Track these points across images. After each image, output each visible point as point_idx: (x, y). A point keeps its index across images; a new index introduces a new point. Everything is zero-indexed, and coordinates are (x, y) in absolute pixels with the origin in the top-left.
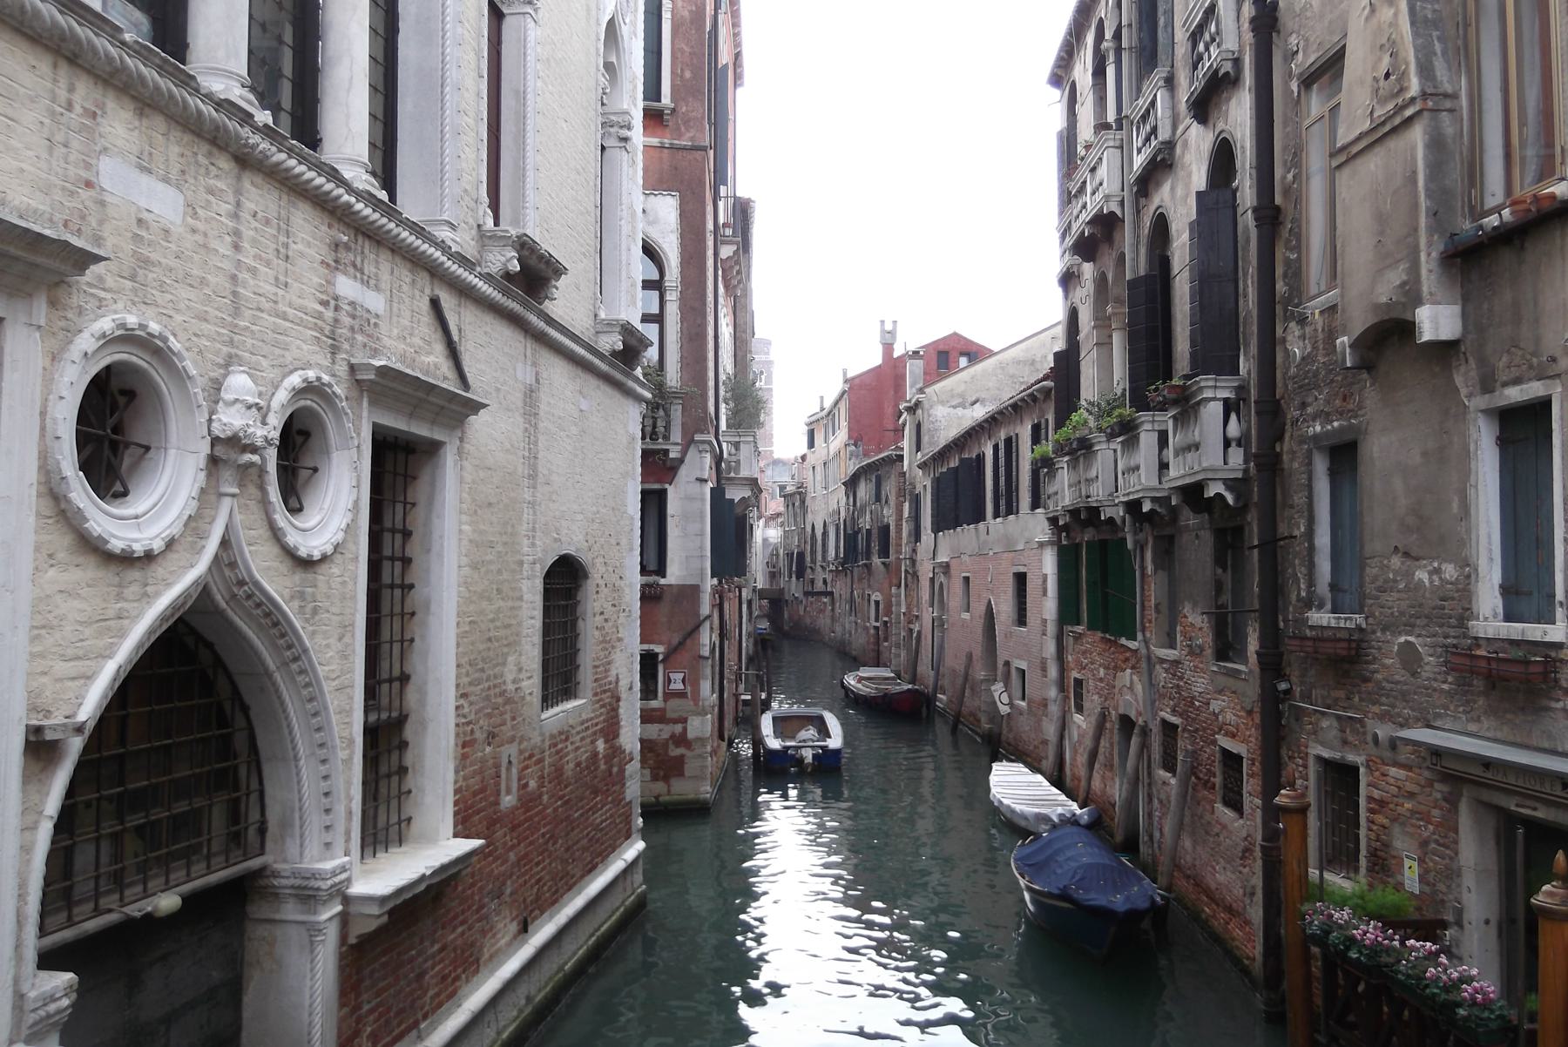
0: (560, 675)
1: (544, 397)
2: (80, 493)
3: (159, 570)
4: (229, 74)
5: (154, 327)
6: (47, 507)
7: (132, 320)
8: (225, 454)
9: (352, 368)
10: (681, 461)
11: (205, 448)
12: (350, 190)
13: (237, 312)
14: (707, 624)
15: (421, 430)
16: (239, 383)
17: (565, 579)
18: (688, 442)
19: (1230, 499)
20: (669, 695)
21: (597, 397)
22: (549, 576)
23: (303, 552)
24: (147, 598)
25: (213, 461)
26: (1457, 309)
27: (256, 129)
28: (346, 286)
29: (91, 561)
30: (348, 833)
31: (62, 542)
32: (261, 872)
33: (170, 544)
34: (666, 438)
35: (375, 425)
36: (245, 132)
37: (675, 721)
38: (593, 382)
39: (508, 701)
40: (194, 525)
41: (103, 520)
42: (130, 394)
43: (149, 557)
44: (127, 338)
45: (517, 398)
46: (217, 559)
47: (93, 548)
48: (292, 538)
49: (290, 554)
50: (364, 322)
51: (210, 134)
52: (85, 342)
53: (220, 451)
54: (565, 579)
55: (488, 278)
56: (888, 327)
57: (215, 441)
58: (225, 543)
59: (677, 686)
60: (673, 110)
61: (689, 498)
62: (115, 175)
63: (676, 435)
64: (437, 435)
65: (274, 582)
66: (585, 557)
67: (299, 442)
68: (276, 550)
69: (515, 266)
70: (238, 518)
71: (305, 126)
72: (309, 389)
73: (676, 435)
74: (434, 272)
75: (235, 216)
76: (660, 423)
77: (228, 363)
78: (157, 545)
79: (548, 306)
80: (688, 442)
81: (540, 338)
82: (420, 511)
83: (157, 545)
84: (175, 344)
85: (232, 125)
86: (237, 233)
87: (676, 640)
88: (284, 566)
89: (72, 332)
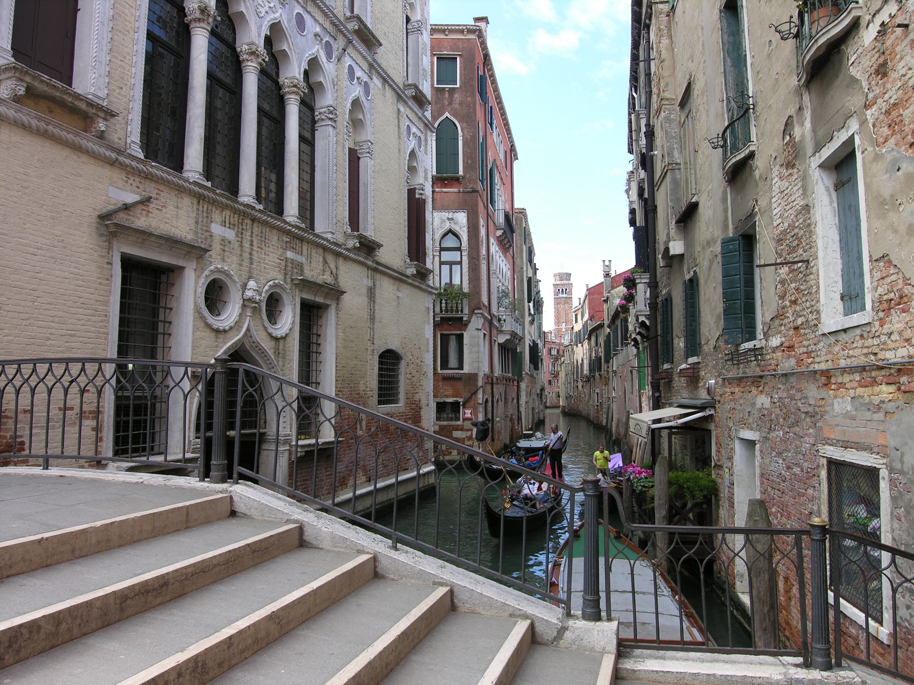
0: (387, 392)
1: (377, 292)
2: (206, 313)
3: (228, 335)
4: (250, 196)
5: (226, 268)
6: (197, 315)
7: (219, 266)
8: (247, 303)
9: (292, 280)
10: (469, 321)
11: (241, 302)
12: (290, 225)
13: (252, 264)
14: (481, 390)
15: (320, 299)
16: (252, 284)
17: (389, 360)
18: (472, 312)
19: (648, 323)
20: (465, 419)
21: (406, 293)
22: (381, 356)
23: (274, 335)
24: (225, 343)
25: (244, 306)
26: (682, 242)
27: (257, 211)
28: (290, 254)
29: (209, 330)
30: (291, 425)
31: (201, 325)
32: (265, 433)
33: (231, 328)
34: (462, 311)
35: (302, 299)
36: (253, 212)
37: (468, 430)
38: (414, 289)
39: (361, 397)
40: (238, 324)
41: (211, 319)
42: (221, 287)
43: (225, 331)
44: (218, 271)
45: (364, 291)
46: (245, 333)
47: (209, 326)
48: (271, 330)
49: (270, 335)
50: (300, 266)
51: (244, 214)
52: (207, 272)
53: (246, 303)
54: (389, 360)
55: (347, 249)
56: (607, 263)
57: (244, 300)
58: (248, 330)
59: (468, 415)
60: (463, 177)
61: (473, 337)
62: (217, 229)
63: (466, 311)
64: (180, 263)
65: (267, 345)
66: (400, 351)
67: (273, 304)
68: (265, 333)
69: (358, 245)
70: (252, 323)
71: (279, 208)
72: (276, 286)
73: (466, 311)
74: (325, 249)
75: (251, 236)
76: (459, 306)
77: (250, 278)
78: (227, 328)
79: (376, 258)
80: (472, 312)
81: (375, 270)
82: (323, 327)
83: (227, 328)
84: (232, 273)
85: (249, 211)
86: (252, 241)
87: (467, 395)
88: (268, 339)
89: (203, 270)
